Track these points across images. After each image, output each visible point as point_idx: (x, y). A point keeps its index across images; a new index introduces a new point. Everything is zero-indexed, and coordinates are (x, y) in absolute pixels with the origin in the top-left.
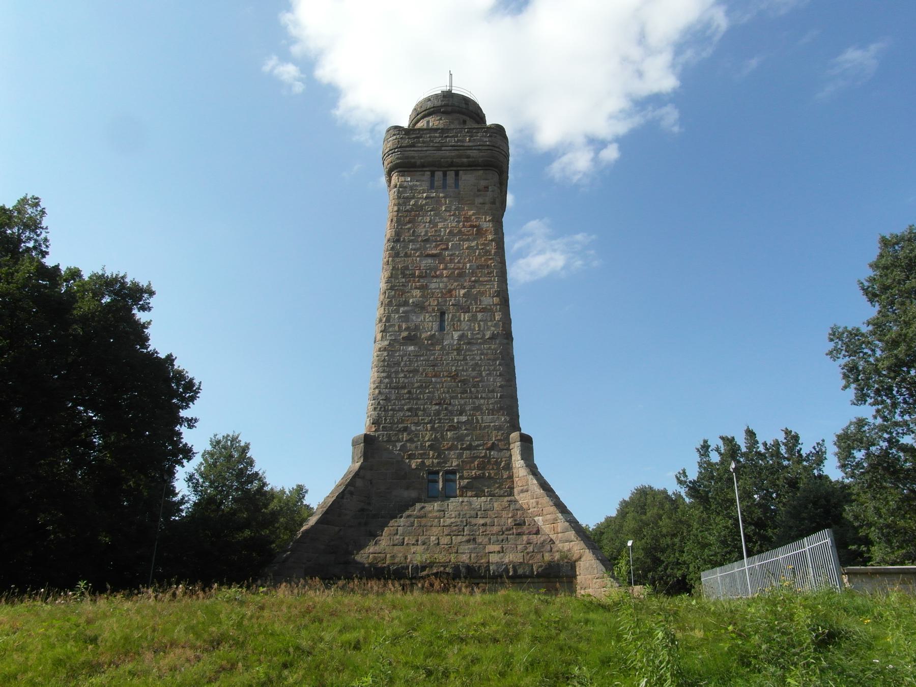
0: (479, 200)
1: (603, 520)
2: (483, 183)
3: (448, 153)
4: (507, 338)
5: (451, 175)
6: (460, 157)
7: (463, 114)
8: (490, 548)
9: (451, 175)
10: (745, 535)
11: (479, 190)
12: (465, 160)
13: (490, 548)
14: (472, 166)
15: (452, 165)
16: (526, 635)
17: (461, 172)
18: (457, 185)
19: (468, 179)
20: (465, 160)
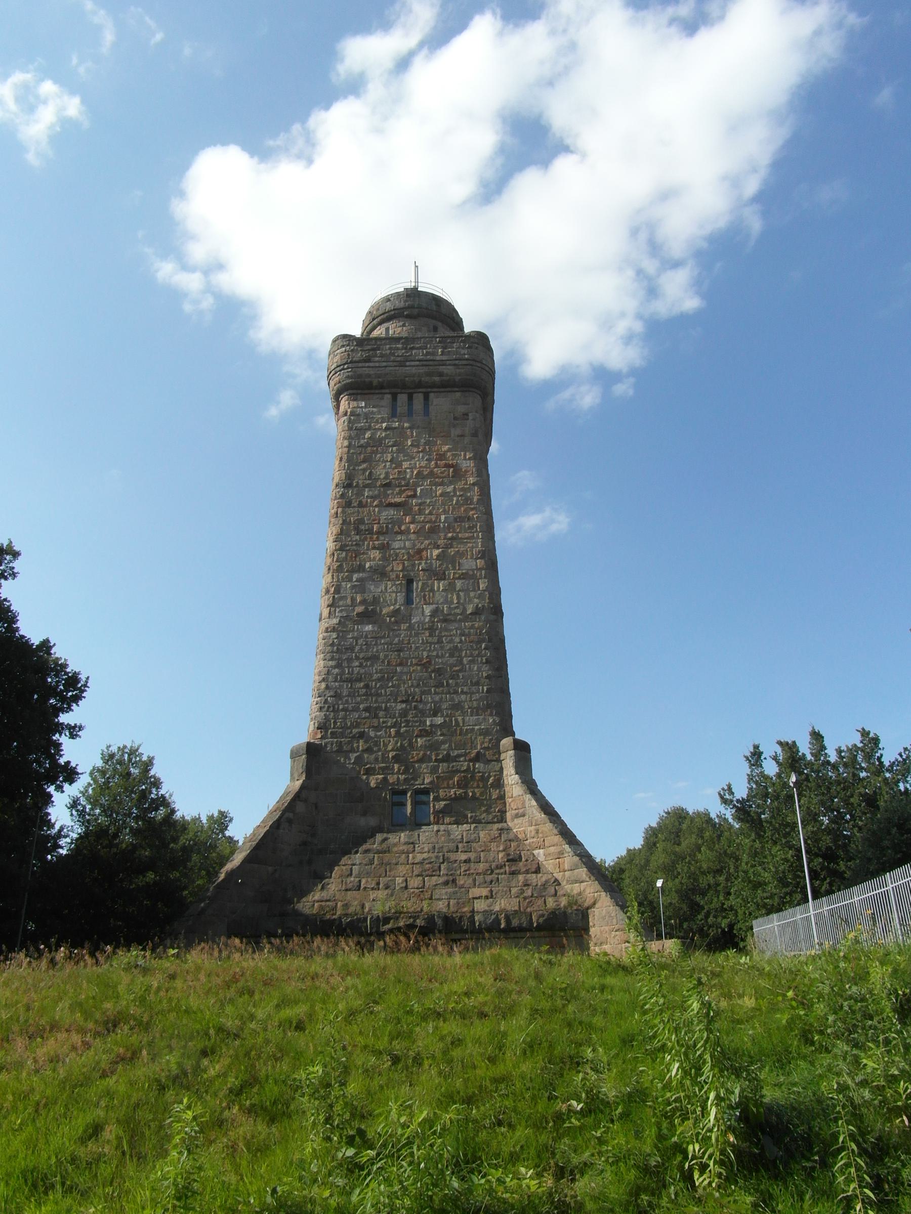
0: (455, 432)
2: (461, 409)
3: (414, 370)
6: (429, 374)
14: (447, 386)
15: (419, 385)
17: (432, 395)
18: (426, 412)
20: (437, 379)
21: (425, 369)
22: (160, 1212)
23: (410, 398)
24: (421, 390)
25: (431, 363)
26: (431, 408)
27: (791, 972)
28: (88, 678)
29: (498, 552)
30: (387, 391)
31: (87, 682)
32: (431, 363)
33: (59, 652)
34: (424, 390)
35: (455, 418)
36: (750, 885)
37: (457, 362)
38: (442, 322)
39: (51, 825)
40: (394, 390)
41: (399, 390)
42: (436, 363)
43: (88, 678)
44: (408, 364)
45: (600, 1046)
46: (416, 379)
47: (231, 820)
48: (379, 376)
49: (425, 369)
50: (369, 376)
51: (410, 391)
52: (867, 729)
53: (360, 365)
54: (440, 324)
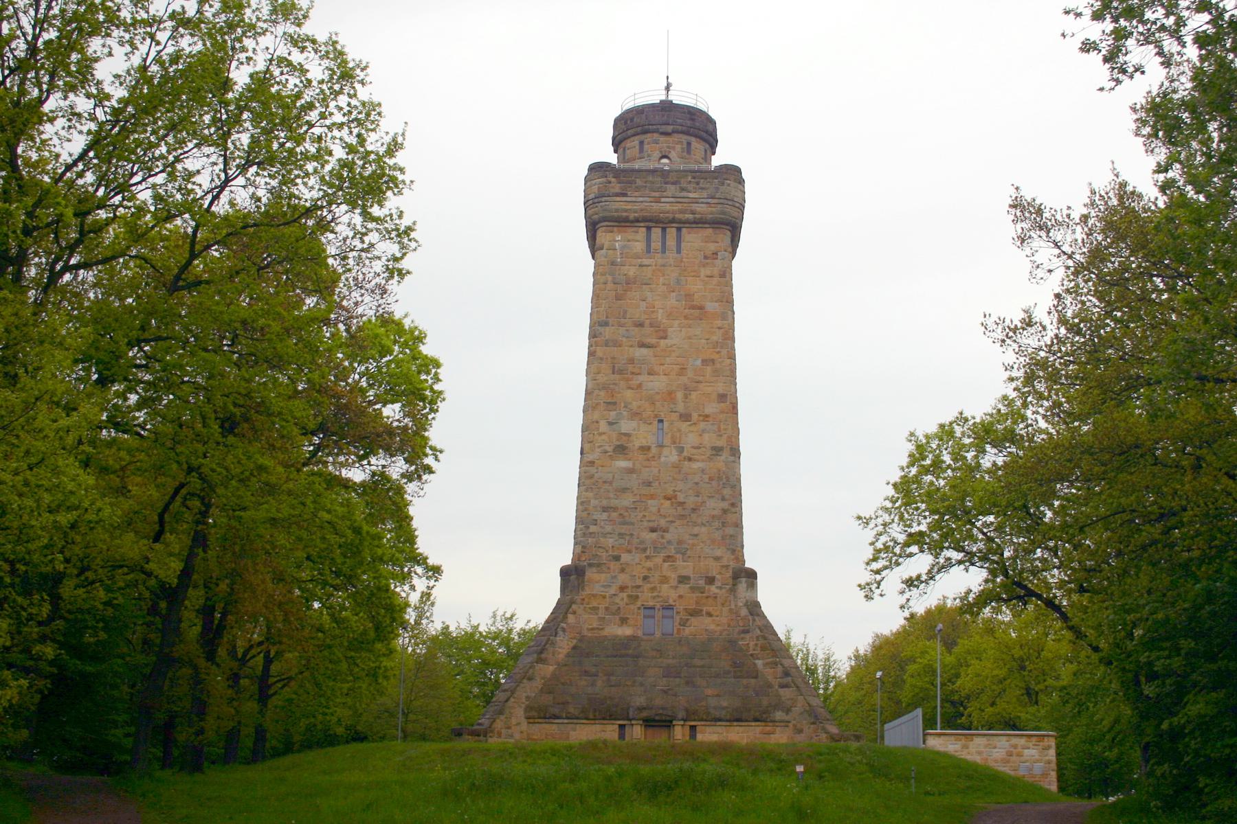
0: (704, 272)
1: (1035, 288)
2: (712, 247)
3: (668, 207)
4: (734, 455)
5: (672, 232)
6: (681, 212)
7: (687, 133)
8: (709, 692)
9: (672, 232)
10: (942, 715)
11: (706, 258)
12: (691, 216)
13: (709, 692)
14: (699, 223)
15: (673, 221)
16: (409, 610)
17: (684, 230)
18: (679, 251)
19: (694, 240)
20: (691, 216)
21: (679, 206)
23: (664, 229)
26: (683, 244)
27: (38, 369)
29: (738, 395)
35: (706, 258)
36: (761, 642)
38: (696, 136)
39: (904, 627)
40: (651, 224)
45: (227, 84)
46: (671, 216)
47: (877, 636)
49: (679, 206)
54: (693, 139)
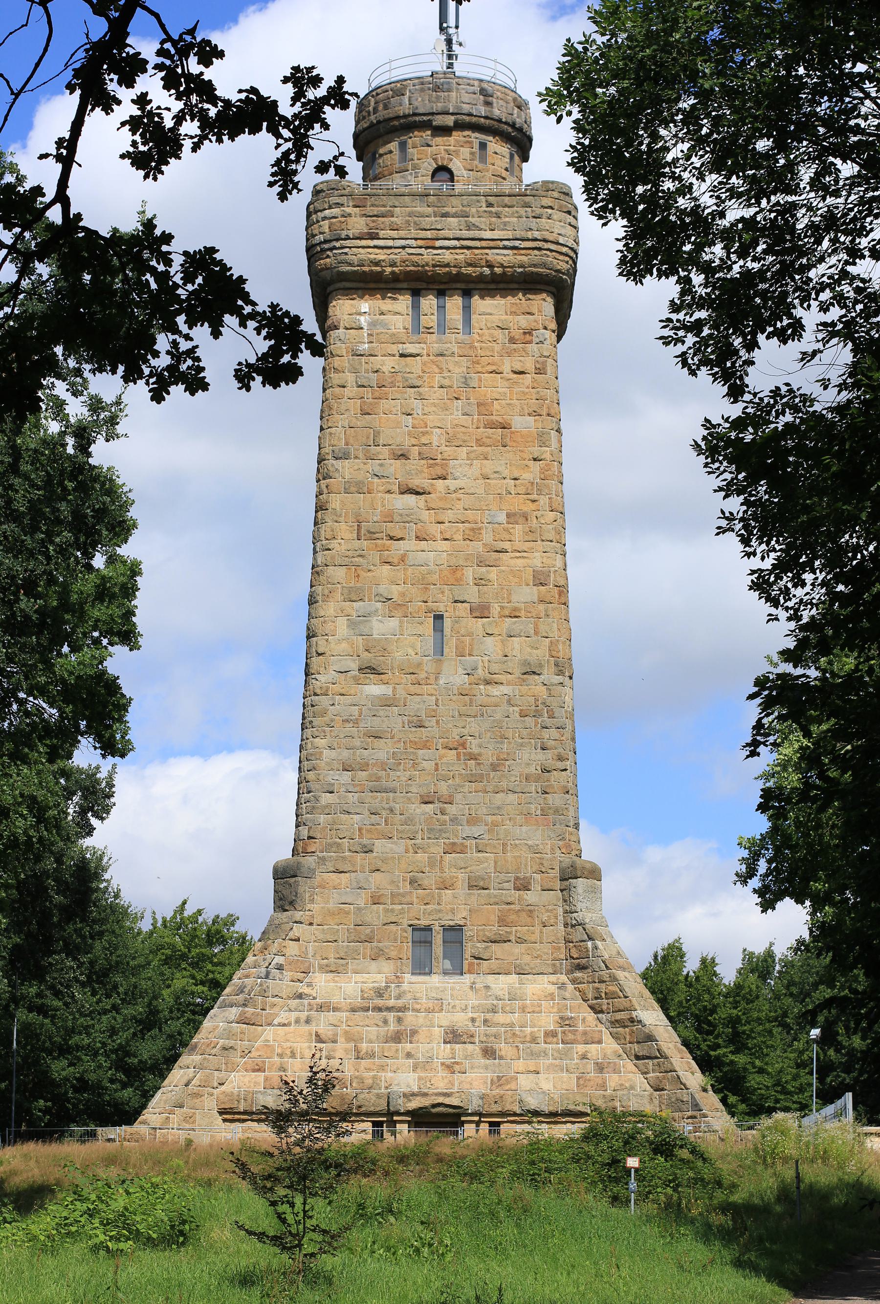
22: (9, 274)
24: (459, 285)
25: (477, 244)
28: (661, 321)
30: (405, 285)
31: (246, 91)
32: (477, 244)
33: (132, 716)
34: (463, 286)
35: (512, 340)
37: (517, 243)
41: (424, 285)
42: (484, 244)
43: (617, 240)
44: (438, 243)
48: (393, 264)
50: (377, 263)
51: (442, 287)
52: (135, 651)
53: (364, 243)
